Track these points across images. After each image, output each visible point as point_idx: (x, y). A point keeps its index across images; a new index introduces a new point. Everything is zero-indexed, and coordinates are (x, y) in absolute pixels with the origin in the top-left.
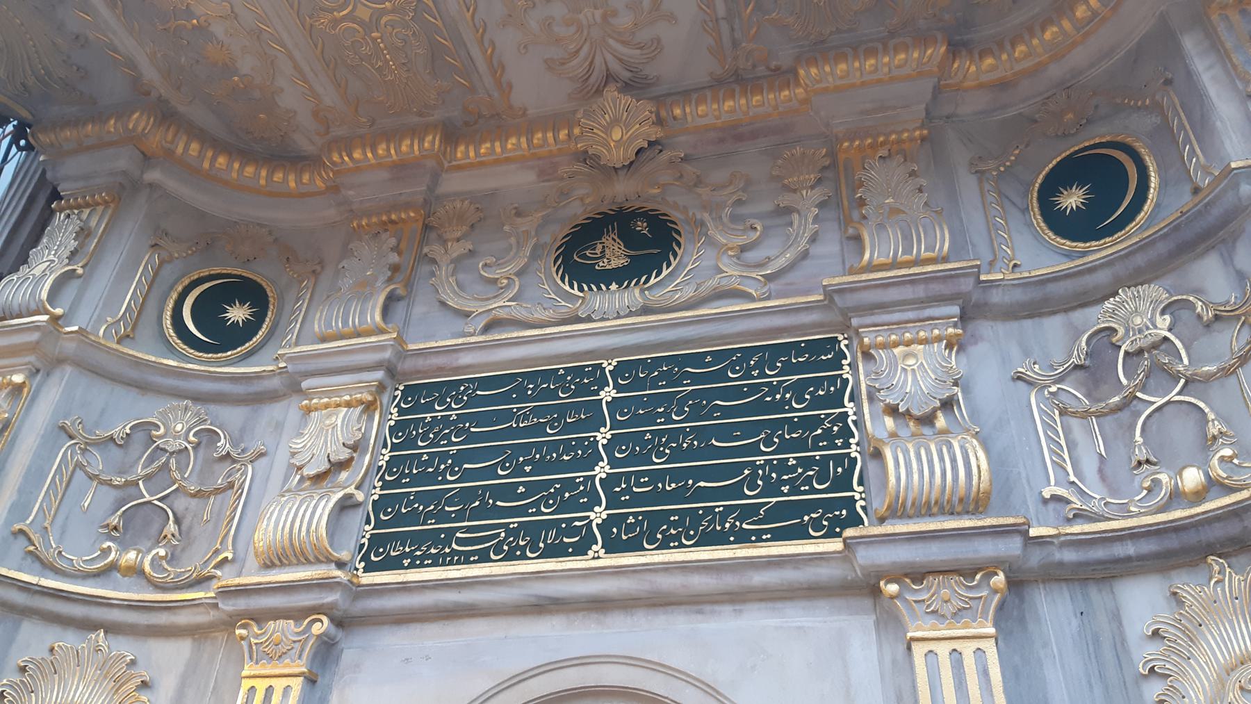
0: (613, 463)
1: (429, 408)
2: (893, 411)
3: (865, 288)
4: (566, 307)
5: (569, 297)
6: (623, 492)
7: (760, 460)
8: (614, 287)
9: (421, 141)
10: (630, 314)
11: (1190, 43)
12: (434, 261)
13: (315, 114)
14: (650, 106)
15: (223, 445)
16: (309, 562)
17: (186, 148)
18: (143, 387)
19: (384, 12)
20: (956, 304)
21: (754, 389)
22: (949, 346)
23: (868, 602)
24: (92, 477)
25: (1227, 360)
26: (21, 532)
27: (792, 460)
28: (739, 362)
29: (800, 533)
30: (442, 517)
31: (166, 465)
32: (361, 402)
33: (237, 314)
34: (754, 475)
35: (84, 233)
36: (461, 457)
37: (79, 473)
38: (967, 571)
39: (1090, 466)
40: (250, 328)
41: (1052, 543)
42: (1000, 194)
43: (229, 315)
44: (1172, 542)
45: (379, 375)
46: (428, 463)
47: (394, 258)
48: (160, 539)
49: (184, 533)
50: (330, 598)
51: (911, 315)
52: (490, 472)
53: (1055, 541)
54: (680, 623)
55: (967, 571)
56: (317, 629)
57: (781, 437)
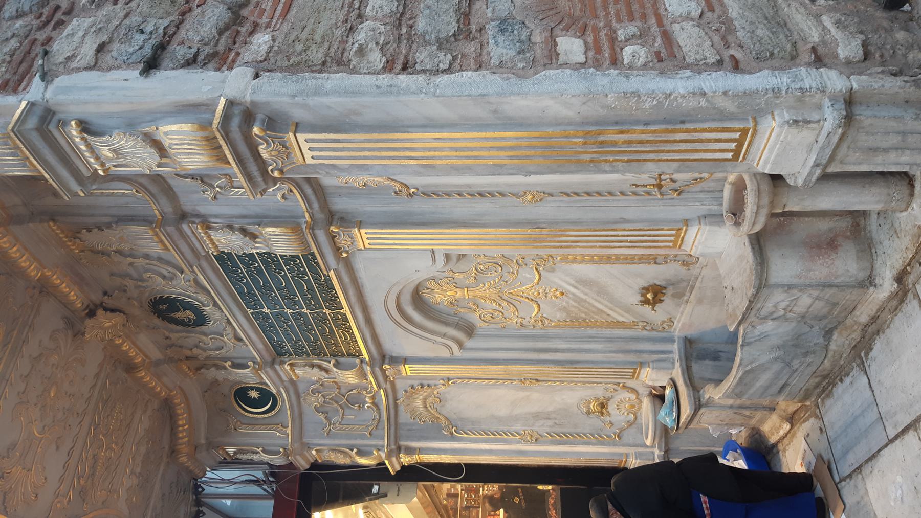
3: (186, 259)
9: (142, 378)
10: (220, 308)
20: (182, 227)
24: (342, 418)
26: (370, 434)
37: (342, 423)
41: (312, 213)
43: (249, 392)
45: (277, 367)
51: (193, 239)
53: (311, 212)
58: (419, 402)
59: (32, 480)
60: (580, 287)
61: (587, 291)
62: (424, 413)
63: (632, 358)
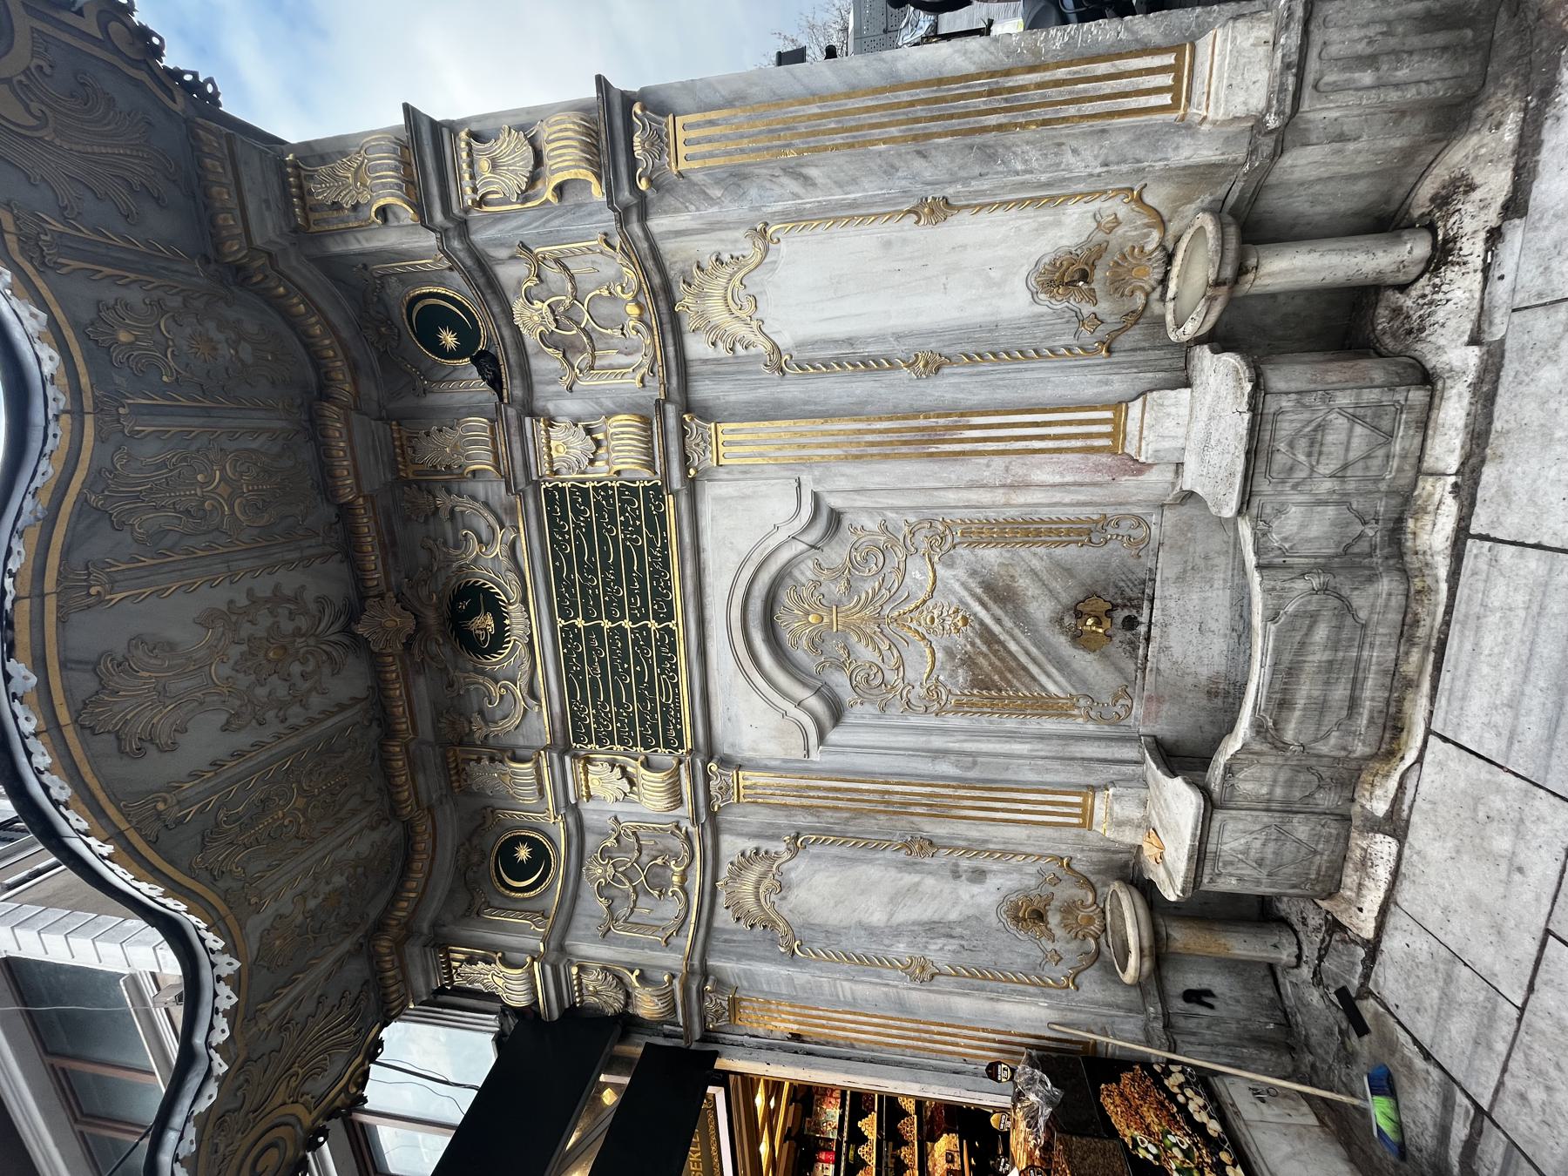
0: (623, 617)
1: (588, 727)
2: (592, 462)
4: (522, 650)
5: (514, 648)
6: (640, 612)
7: (621, 536)
8: (507, 622)
10: (528, 611)
11: (336, 247)
12: (486, 737)
13: (373, 829)
14: (370, 602)
15: (611, 842)
16: (679, 780)
17: (403, 909)
18: (576, 897)
19: (300, 788)
21: (577, 537)
22: (551, 426)
23: (698, 484)
25: (564, 276)
27: (620, 519)
28: (559, 546)
29: (662, 517)
30: (654, 711)
31: (623, 873)
32: (585, 766)
33: (523, 853)
34: (631, 540)
35: (471, 960)
36: (619, 704)
37: (630, 920)
38: (683, 433)
39: (624, 360)
40: (532, 842)
42: (441, 381)
44: (667, 327)
45: (567, 759)
46: (622, 722)
47: (485, 762)
48: (665, 865)
49: (662, 852)
50: (699, 764)
52: (628, 687)
54: (710, 579)
55: (683, 433)
56: (714, 768)
57: (607, 524)
58: (747, 888)
59: (155, 721)
60: (991, 604)
61: (999, 612)
62: (754, 909)
63: (1077, 776)
